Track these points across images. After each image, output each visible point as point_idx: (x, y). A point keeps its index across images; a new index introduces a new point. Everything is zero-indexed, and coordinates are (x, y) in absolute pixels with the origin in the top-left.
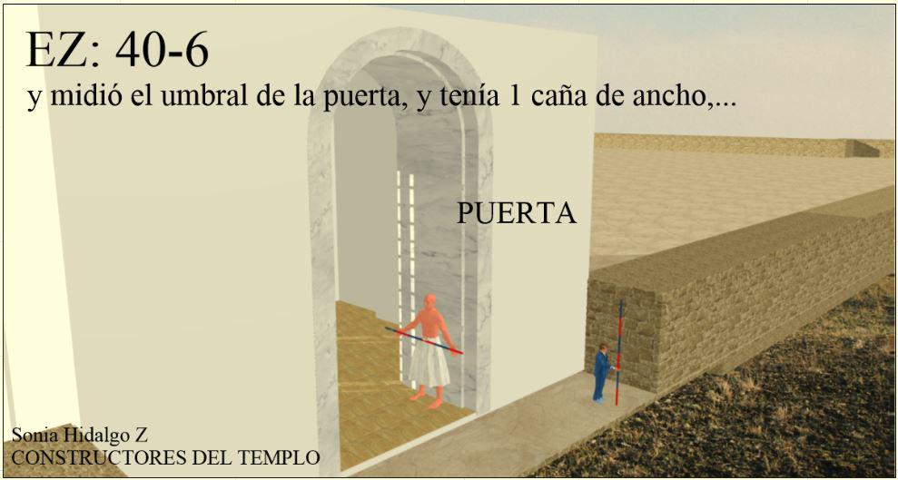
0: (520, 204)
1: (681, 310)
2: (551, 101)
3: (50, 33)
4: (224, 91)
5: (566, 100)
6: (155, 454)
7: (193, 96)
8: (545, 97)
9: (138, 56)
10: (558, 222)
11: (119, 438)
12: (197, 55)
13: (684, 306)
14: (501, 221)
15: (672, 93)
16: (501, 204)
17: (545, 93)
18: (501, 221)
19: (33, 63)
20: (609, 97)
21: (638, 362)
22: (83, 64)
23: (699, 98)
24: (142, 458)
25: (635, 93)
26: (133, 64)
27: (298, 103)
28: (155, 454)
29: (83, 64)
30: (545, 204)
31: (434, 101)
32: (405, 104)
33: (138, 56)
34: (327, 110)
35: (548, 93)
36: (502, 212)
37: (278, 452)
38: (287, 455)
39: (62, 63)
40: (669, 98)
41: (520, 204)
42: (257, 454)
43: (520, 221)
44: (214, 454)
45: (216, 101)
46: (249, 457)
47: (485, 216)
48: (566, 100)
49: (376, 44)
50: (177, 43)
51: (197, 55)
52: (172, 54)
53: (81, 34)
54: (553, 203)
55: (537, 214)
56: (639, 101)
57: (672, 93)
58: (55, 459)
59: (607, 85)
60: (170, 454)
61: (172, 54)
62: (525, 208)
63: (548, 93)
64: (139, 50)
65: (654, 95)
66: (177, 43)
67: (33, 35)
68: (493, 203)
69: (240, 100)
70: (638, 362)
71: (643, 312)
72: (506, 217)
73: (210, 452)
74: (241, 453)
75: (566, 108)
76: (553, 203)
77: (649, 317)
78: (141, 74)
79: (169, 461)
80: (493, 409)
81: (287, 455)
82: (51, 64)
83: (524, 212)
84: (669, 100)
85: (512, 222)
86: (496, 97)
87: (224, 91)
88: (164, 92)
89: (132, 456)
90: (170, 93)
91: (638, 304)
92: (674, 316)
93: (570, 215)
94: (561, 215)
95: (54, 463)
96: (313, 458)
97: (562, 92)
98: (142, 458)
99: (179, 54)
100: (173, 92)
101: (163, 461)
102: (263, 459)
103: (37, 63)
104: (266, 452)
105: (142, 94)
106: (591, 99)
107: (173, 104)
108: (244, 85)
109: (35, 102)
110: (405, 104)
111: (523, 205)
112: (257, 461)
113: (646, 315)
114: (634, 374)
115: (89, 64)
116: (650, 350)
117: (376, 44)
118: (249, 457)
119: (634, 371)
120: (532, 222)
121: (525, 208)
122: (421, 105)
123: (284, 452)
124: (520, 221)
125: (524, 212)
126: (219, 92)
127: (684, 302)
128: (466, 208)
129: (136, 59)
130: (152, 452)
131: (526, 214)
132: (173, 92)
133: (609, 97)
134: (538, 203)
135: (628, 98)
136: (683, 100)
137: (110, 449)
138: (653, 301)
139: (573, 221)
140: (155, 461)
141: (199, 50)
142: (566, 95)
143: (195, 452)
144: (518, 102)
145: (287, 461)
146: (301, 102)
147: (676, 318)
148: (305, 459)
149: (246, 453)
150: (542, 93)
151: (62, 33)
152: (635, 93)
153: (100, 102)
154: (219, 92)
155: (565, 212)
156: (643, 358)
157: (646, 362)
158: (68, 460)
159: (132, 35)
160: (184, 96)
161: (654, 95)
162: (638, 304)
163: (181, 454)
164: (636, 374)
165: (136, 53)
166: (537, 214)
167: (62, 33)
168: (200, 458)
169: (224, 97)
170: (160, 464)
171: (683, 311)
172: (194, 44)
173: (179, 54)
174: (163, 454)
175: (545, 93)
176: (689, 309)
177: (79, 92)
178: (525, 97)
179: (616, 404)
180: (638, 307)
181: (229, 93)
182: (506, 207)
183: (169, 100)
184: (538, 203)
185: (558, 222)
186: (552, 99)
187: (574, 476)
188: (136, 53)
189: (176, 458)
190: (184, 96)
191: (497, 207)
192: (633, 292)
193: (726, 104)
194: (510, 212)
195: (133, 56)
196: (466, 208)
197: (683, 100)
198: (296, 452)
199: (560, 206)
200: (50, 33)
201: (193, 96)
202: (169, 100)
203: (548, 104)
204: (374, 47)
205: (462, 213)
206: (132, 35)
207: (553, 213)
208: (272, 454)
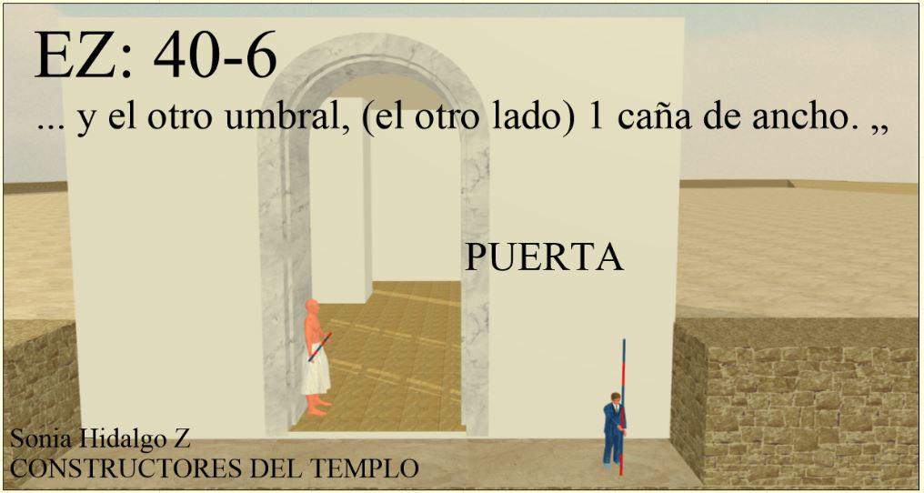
0: (549, 245)
1: (40, 368)
2: (644, 123)
3: (67, 34)
4: (309, 111)
5: (664, 122)
6: (201, 464)
7: (267, 117)
8: (636, 118)
9: (183, 63)
10: (600, 268)
11: (152, 443)
12: (262, 61)
13: (45, 362)
14: (524, 268)
15: (805, 113)
16: (524, 245)
17: (636, 113)
18: (524, 268)
19: (254, 476)
20: (721, 118)
21: (816, 447)
22: (111, 74)
23: (839, 119)
24: (183, 469)
25: (756, 114)
26: (176, 74)
27: (497, 126)
28: (201, 464)
29: (111, 74)
30: (582, 245)
31: (100, 122)
32: (345, 127)
33: (183, 63)
34: (471, 268)
35: (639, 114)
36: (524, 256)
37: (363, 461)
38: (376, 464)
39: (82, 73)
40: (801, 119)
41: (549, 245)
42: (335, 464)
43: (549, 268)
44: (278, 464)
45: (298, 123)
46: (325, 467)
47: (503, 260)
48: (664, 122)
49: (330, 51)
50: (234, 46)
51: (262, 61)
52: (228, 61)
53: (108, 35)
54: (592, 244)
55: (570, 258)
56: (760, 123)
57: (805, 113)
58: (69, 469)
59: (718, 102)
60: (220, 464)
61: (228, 61)
62: (555, 250)
63: (639, 114)
64: (184, 54)
65: (781, 117)
66: (234, 46)
67: (44, 35)
68: (512, 244)
69: (330, 122)
70: (816, 447)
71: (824, 377)
72: (530, 262)
73: (274, 461)
74: (315, 462)
75: (664, 131)
76: (592, 244)
77: (833, 382)
78: (187, 90)
79: (220, 473)
80: (491, 436)
81: (376, 464)
82: (68, 75)
83: (554, 256)
84: (800, 122)
85: (538, 269)
86: (687, 117)
87: (309, 111)
88: (229, 112)
89: (170, 465)
90: (237, 114)
91: (816, 368)
92: (31, 377)
93: (615, 259)
94: (603, 260)
95: (67, 474)
96: (409, 469)
97: (658, 113)
98: (183, 469)
99: (239, 61)
100: (240, 112)
101: (210, 473)
102: (343, 470)
103: (50, 72)
104: (348, 461)
105: (390, 115)
106: (697, 120)
107: (240, 126)
108: (131, 103)
109: (87, 125)
110: (345, 127)
111: (552, 247)
112: (335, 473)
113: (828, 381)
114: (810, 466)
115: (118, 73)
116: (835, 428)
117: (330, 51)
118: (325, 467)
119: (812, 463)
120: (564, 268)
121: (555, 250)
122: (82, 128)
123: (372, 461)
124: (549, 268)
125: (554, 256)
126: (302, 113)
127: (45, 357)
128: (477, 251)
129: (181, 67)
130: (197, 461)
131: (556, 257)
132: (240, 112)
133: (721, 118)
134: (573, 244)
135: (747, 119)
136: (819, 122)
137: (140, 457)
138: (839, 360)
139: (618, 268)
140: (200, 472)
141: (264, 54)
142: (664, 117)
143: (254, 461)
144: (402, 125)
145: (375, 472)
146: (502, 124)
147: (35, 380)
148: (399, 470)
149: (322, 462)
150: (631, 113)
151: (83, 34)
152: (756, 114)
153: (332, 125)
154: (302, 113)
155: (609, 256)
156: (824, 441)
157: (828, 445)
158: (86, 472)
159: (176, 36)
160: (255, 117)
161: (781, 117)
162: (816, 368)
163: (235, 463)
164: (814, 466)
165: (181, 58)
166: (570, 258)
167: (83, 34)
168: (260, 468)
169: (309, 119)
170: (207, 476)
171: (45, 369)
172: (257, 48)
173: (239, 61)
174: (211, 464)
175: (636, 113)
176: (55, 365)
177: (56, 436)
178: (608, 117)
179: (624, 341)
180: (816, 372)
181: (315, 114)
182: (530, 250)
183: (234, 122)
184: (573, 244)
185: (600, 268)
186: (646, 120)
187: (754, 483)
188: (181, 58)
189: (228, 469)
190: (255, 117)
191: (518, 249)
192: (808, 354)
193: (51, 127)
194: (535, 256)
195: (176, 63)
196: (477, 251)
197: (819, 122)
198: (387, 460)
199: (601, 249)
200: (67, 34)
201: (267, 117)
202: (234, 122)
203: (639, 126)
204: (329, 53)
205: (471, 257)
206: (176, 36)
207: (593, 257)
208: (355, 465)
